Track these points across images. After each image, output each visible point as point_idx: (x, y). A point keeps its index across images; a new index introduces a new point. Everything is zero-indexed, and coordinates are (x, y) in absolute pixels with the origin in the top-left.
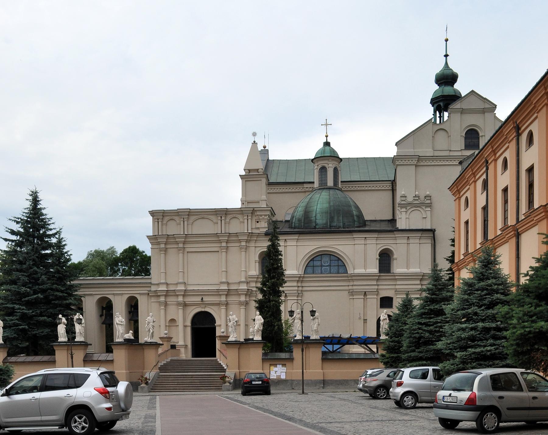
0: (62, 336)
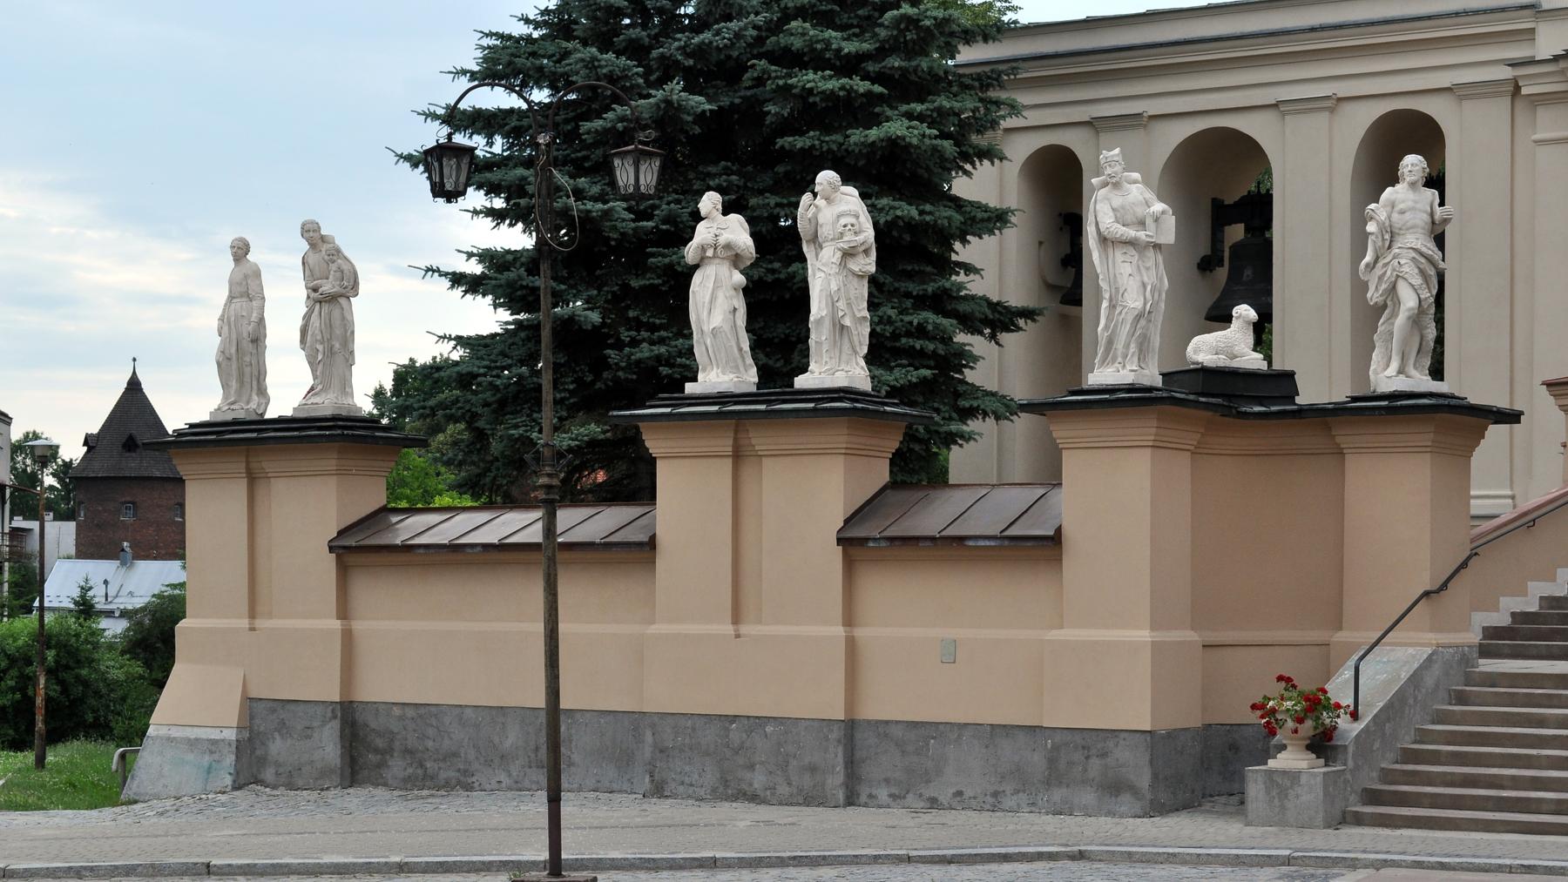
0: (723, 363)
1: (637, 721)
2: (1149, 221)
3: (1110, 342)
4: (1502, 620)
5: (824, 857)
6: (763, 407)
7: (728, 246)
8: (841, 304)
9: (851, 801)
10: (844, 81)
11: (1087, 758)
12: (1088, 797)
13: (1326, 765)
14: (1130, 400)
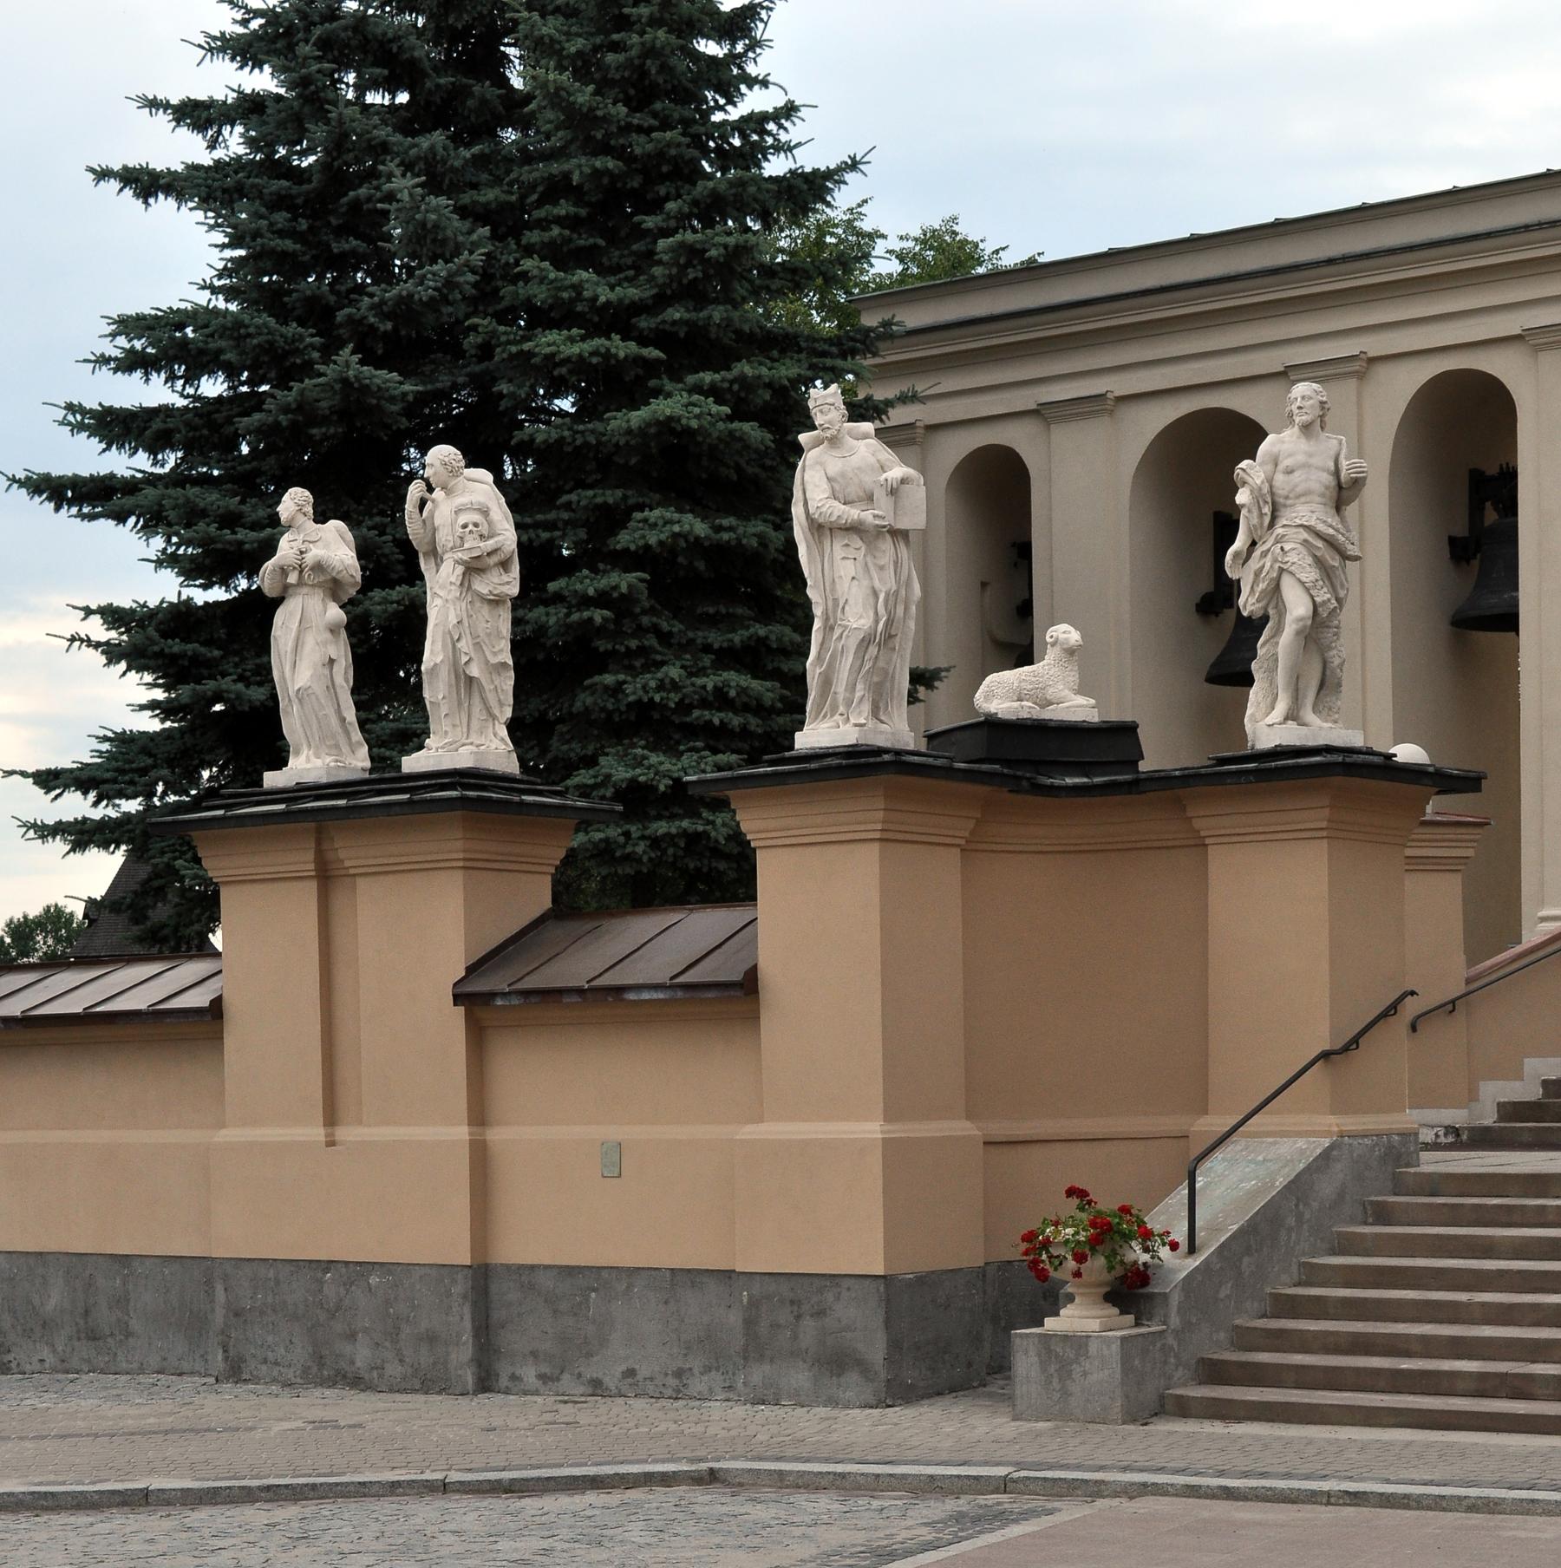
1: (205, 1268)
2: (880, 495)
3: (827, 682)
4: (1527, 1090)
5: (314, 1487)
6: (342, 802)
7: (319, 567)
8: (463, 645)
9: (485, 1384)
10: (598, 342)
11: (798, 1317)
12: (800, 1377)
13: (1137, 1324)
14: (856, 765)
